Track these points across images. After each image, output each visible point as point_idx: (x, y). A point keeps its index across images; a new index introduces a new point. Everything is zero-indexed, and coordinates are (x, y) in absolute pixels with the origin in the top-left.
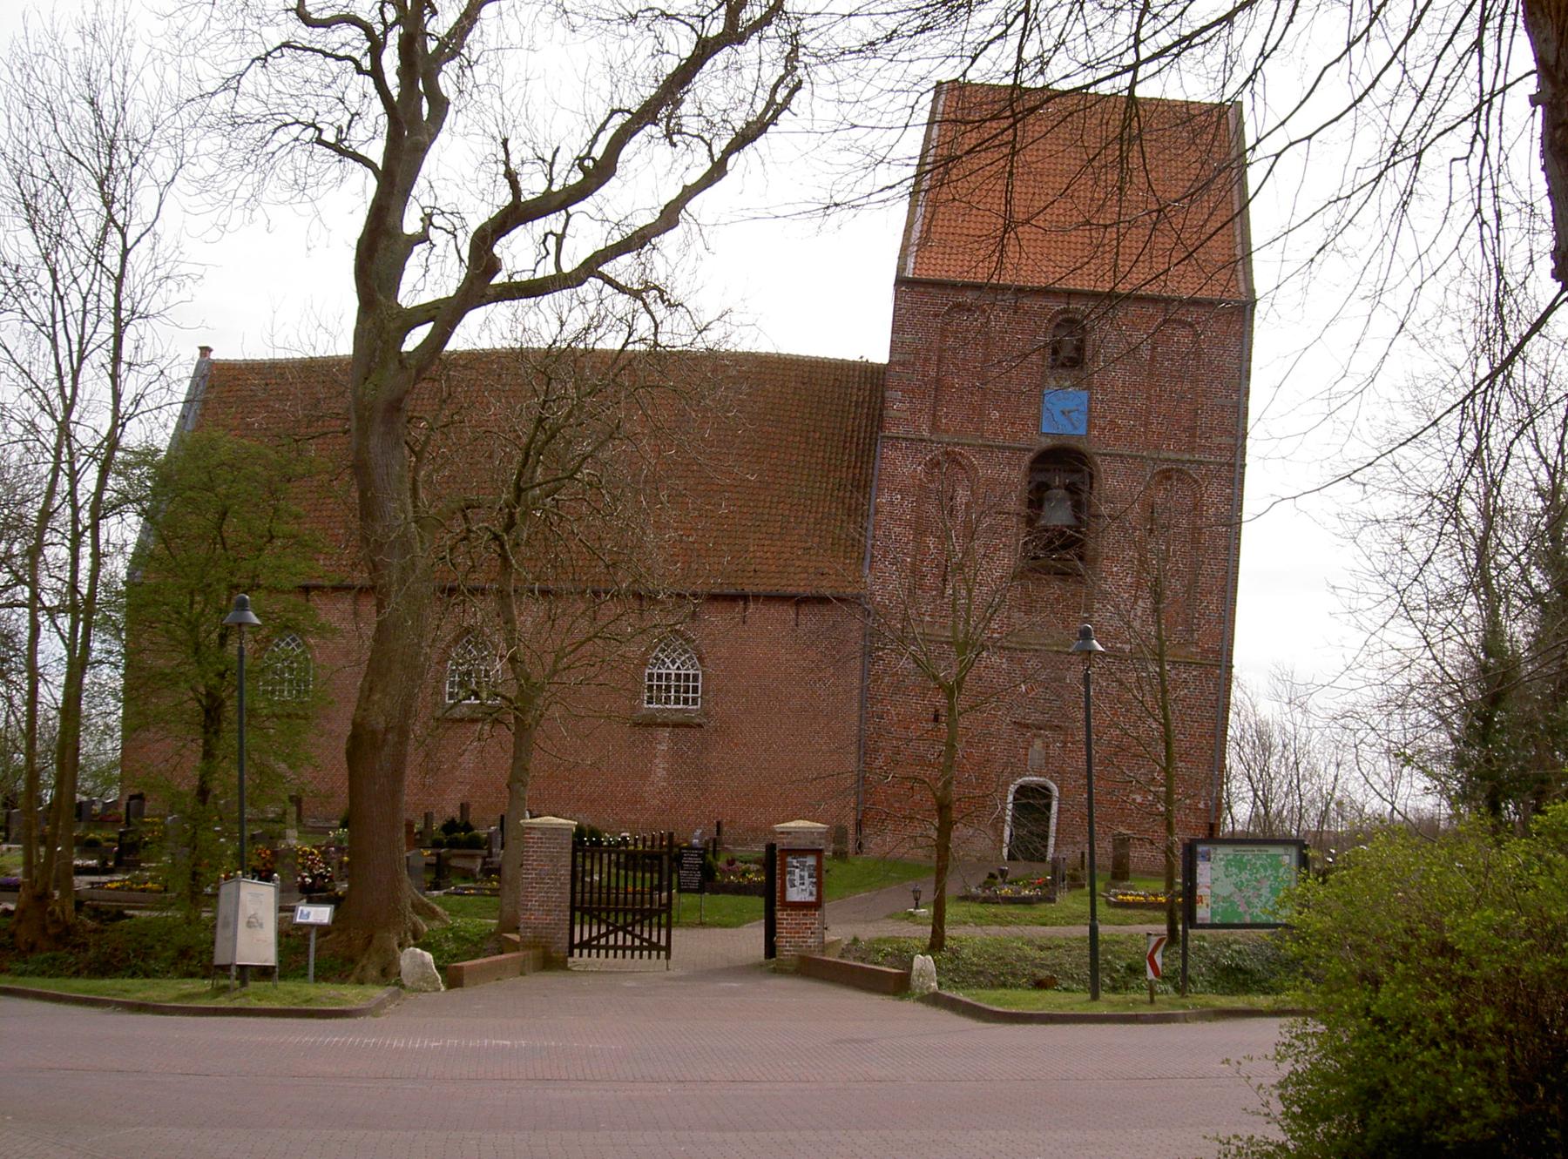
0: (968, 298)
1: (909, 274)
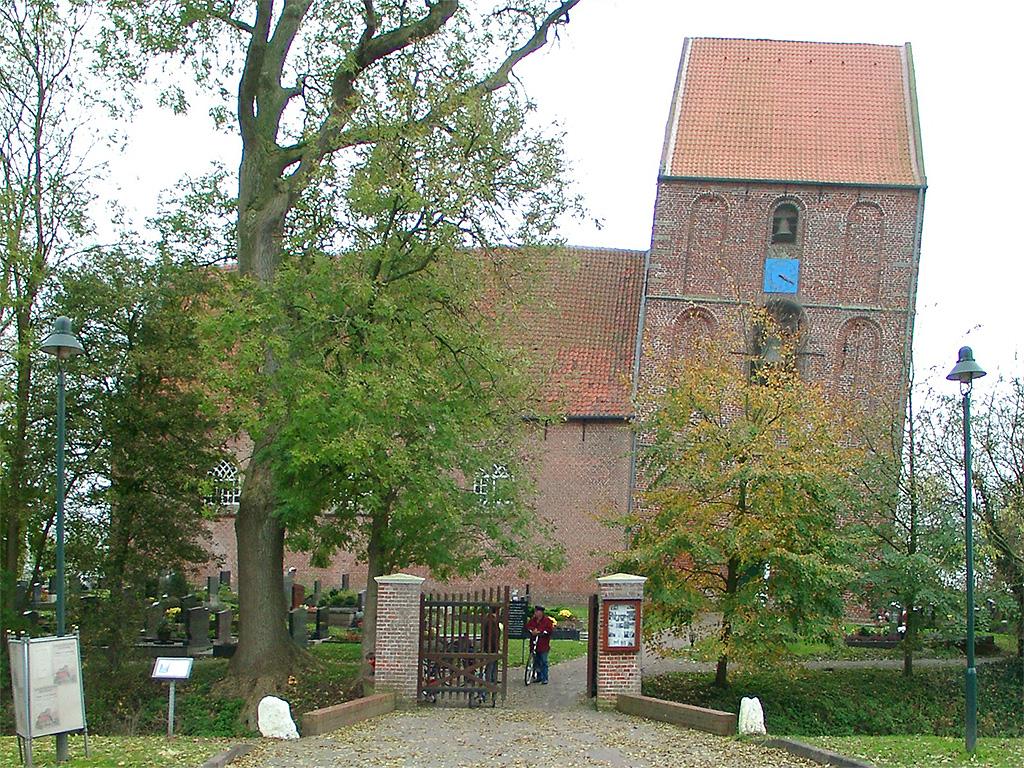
0: (713, 190)
1: (668, 173)
